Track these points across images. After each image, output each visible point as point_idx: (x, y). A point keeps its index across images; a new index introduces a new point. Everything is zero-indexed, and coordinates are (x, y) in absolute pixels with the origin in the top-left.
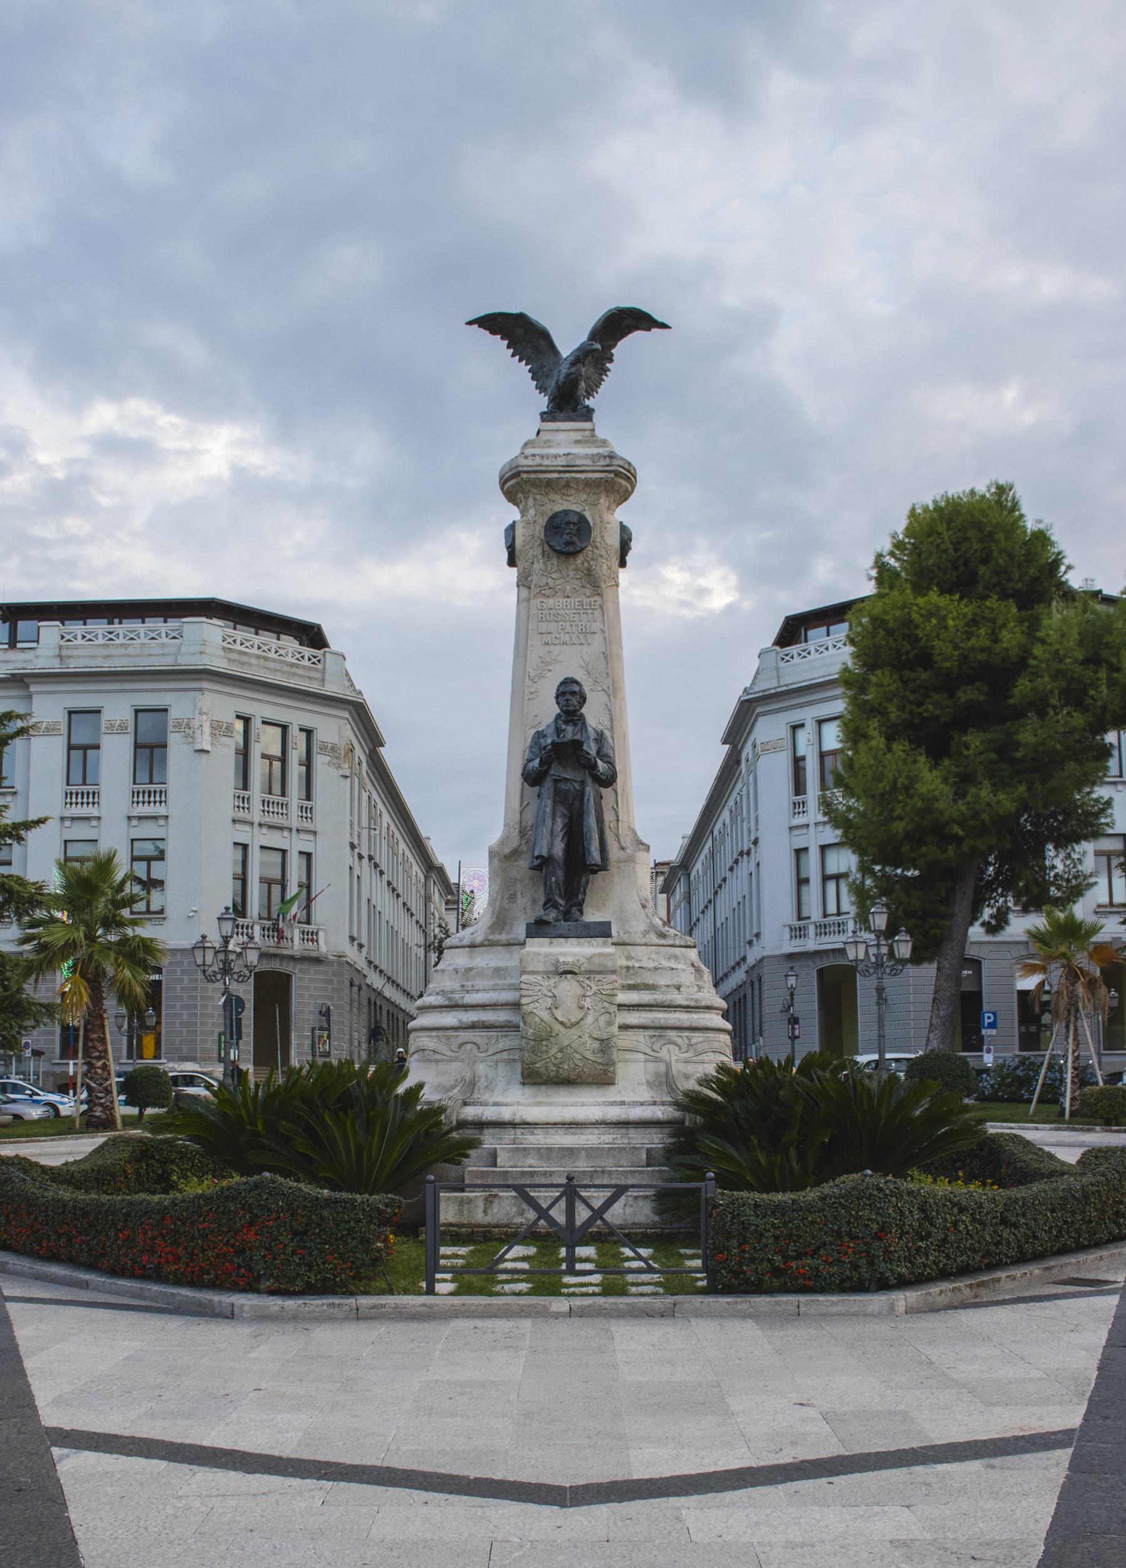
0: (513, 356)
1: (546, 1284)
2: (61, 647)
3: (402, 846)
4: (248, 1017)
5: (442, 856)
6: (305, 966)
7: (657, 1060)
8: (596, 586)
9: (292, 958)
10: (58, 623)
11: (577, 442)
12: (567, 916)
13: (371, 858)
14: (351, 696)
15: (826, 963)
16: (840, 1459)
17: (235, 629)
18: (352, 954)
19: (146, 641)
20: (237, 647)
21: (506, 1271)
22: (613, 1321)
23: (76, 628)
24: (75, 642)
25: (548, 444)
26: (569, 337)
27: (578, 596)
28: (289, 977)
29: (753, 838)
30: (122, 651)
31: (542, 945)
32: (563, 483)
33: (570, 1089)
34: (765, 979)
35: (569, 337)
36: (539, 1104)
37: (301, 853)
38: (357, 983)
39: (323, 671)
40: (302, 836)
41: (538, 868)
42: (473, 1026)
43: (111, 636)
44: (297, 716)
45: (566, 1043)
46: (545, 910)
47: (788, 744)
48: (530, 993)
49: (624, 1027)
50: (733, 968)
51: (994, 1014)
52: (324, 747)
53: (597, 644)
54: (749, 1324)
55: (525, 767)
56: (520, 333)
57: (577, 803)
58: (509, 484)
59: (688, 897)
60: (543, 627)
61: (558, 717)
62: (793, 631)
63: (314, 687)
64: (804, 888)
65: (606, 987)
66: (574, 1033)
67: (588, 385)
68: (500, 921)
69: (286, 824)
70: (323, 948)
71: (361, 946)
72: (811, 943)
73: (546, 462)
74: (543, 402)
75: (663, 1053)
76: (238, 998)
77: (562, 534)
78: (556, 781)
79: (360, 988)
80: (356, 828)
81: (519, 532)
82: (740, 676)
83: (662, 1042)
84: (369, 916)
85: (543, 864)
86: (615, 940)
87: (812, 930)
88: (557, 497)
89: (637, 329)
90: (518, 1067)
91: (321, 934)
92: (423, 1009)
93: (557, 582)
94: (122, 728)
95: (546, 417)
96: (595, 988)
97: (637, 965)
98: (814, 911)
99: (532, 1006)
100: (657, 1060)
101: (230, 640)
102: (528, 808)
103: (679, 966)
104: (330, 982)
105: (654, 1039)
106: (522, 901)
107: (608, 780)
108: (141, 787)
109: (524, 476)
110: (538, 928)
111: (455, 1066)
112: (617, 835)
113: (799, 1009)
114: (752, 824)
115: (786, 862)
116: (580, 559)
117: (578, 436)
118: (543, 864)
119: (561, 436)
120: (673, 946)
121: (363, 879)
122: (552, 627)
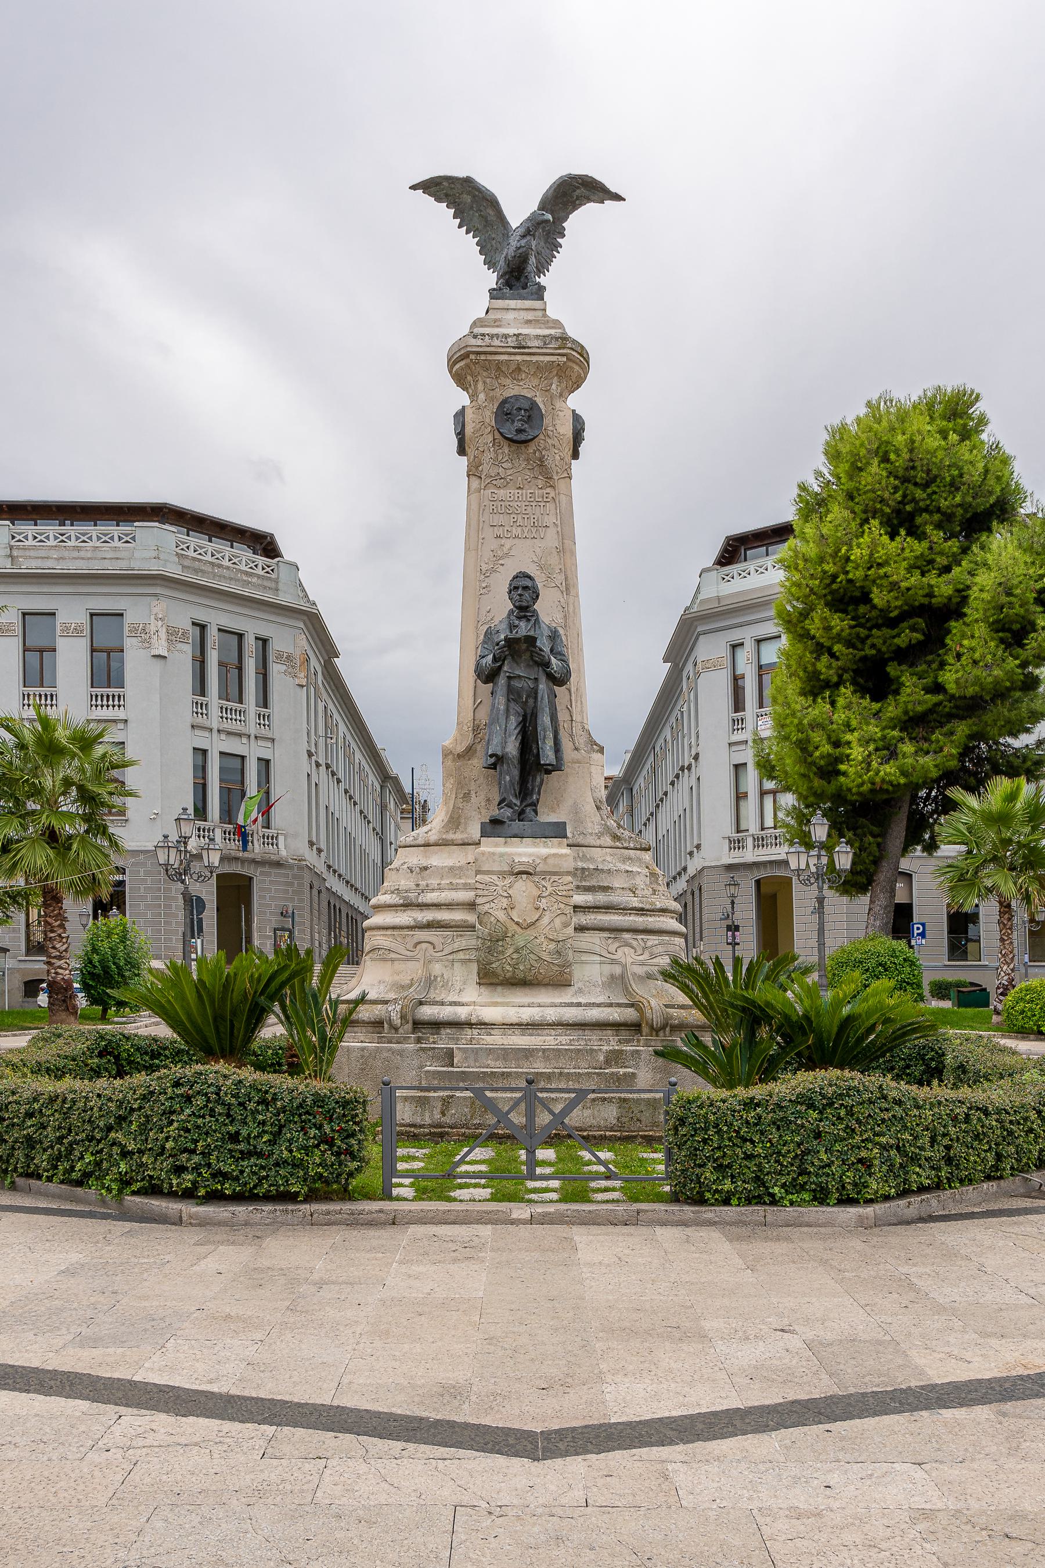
0: (460, 227)
1: (507, 1185)
2: (11, 548)
3: (358, 756)
4: (210, 917)
5: (397, 767)
6: (267, 869)
7: (613, 962)
8: (550, 477)
9: (254, 861)
10: (8, 522)
11: (528, 322)
12: (521, 815)
13: (328, 766)
14: (304, 606)
15: (763, 874)
16: (830, 1401)
17: (188, 535)
18: (311, 857)
19: (98, 544)
20: (191, 553)
21: (467, 1175)
22: (575, 1228)
23: (27, 528)
24: (27, 543)
25: (497, 323)
26: (518, 207)
27: (530, 488)
28: (251, 879)
29: (693, 753)
30: (76, 554)
31: (497, 845)
32: (513, 367)
33: (527, 990)
34: (704, 888)
35: (518, 207)
36: (495, 1004)
37: (259, 759)
38: (317, 886)
39: (276, 581)
40: (260, 743)
41: (493, 766)
42: (429, 925)
43: (63, 538)
44: (252, 626)
45: (522, 944)
46: (499, 809)
47: (728, 662)
48: (486, 893)
49: (581, 929)
50: (675, 878)
51: (923, 925)
52: (279, 656)
53: (551, 539)
55: (478, 665)
56: (464, 199)
57: (531, 701)
58: (457, 366)
59: (631, 812)
60: (498, 519)
61: (511, 612)
62: (735, 550)
63: (268, 596)
64: (742, 803)
65: (561, 888)
66: (531, 933)
67: (538, 261)
68: (455, 821)
69: (244, 730)
70: (284, 853)
71: (319, 851)
72: (750, 855)
73: (496, 342)
74: (491, 279)
76: (198, 898)
77: (513, 421)
78: (509, 678)
79: (319, 892)
80: (313, 737)
81: (469, 415)
83: (617, 944)
84: (327, 822)
85: (497, 762)
86: (570, 841)
87: (750, 841)
88: (507, 382)
89: (589, 200)
90: (474, 967)
91: (281, 839)
92: (379, 908)
93: (509, 472)
94: (78, 631)
95: (495, 294)
96: (550, 889)
97: (592, 867)
98: (751, 824)
99: (487, 906)
100: (613, 962)
101: (184, 546)
102: (481, 706)
103: (635, 869)
104: (291, 884)
105: (610, 941)
107: (560, 680)
109: (472, 357)
110: (494, 827)
111: (410, 964)
112: (571, 735)
114: (693, 740)
115: (726, 776)
116: (532, 447)
117: (530, 316)
118: (497, 762)
119: (511, 315)
120: (627, 848)
121: (320, 786)
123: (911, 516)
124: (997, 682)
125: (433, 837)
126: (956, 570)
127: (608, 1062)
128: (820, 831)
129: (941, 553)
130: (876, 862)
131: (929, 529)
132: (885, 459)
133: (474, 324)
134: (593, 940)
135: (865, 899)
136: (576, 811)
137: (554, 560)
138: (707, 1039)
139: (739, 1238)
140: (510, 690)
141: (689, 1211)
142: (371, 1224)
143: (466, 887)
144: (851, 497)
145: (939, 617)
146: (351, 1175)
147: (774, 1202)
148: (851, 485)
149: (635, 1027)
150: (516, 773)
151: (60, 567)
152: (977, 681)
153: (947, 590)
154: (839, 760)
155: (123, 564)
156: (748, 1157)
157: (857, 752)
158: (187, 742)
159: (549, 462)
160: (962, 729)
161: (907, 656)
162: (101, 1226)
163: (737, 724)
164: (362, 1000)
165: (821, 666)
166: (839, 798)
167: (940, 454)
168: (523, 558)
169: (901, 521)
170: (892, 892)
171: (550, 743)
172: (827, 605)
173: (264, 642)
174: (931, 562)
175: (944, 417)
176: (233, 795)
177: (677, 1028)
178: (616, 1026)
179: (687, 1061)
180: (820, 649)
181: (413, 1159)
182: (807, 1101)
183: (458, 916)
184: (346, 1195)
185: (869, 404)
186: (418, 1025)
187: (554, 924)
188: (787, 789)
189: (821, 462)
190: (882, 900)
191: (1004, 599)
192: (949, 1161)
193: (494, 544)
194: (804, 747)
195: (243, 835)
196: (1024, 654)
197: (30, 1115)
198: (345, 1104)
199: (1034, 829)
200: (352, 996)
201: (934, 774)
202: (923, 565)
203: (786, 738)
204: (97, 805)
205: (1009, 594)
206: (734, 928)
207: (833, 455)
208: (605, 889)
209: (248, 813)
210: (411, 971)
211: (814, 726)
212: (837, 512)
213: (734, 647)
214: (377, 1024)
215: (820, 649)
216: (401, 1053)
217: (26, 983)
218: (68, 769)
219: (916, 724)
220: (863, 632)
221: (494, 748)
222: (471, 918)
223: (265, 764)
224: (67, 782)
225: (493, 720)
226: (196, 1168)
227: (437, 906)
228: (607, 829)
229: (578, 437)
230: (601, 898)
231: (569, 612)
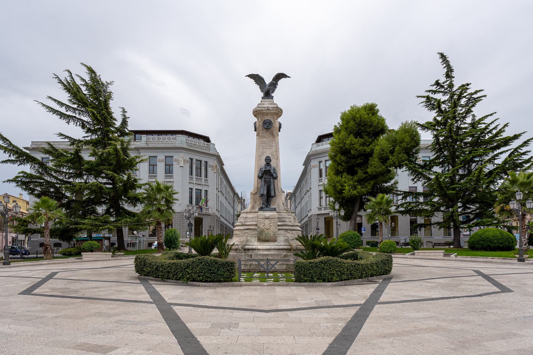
3: (228, 189)
5: (238, 191)
8: (274, 136)
12: (267, 207)
14: (216, 154)
18: (217, 213)
23: (150, 137)
25: (263, 104)
26: (268, 80)
35: (268, 80)
38: (218, 220)
42: (247, 229)
44: (203, 159)
49: (279, 230)
52: (210, 166)
53: (274, 149)
54: (303, 287)
56: (257, 79)
60: (263, 145)
62: (320, 139)
63: (207, 152)
66: (269, 230)
68: (253, 208)
72: (323, 212)
74: (262, 95)
75: (287, 235)
82: (307, 150)
85: (262, 195)
94: (162, 161)
95: (263, 98)
98: (324, 204)
106: (258, 203)
107: (276, 178)
108: (167, 175)
110: (261, 209)
113: (320, 226)
117: (270, 103)
119: (266, 103)
122: (264, 145)
123: (361, 133)
124: (380, 171)
125: (248, 211)
126: (371, 146)
127: (284, 257)
128: (337, 207)
129: (368, 142)
130: (352, 213)
131: (365, 136)
132: (354, 120)
133: (258, 105)
134: (282, 232)
135: (349, 222)
136: (278, 205)
137: (275, 153)
138: (305, 252)
139: (309, 289)
140: (265, 181)
141: (298, 283)
142: (236, 286)
143: (255, 221)
144: (346, 129)
145: (367, 156)
146: (232, 277)
147: (315, 282)
148: (347, 126)
149: (290, 250)
150: (266, 198)
151: (158, 146)
152: (376, 171)
153: (369, 150)
154: (343, 190)
155: (173, 145)
156: (310, 273)
157: (347, 188)
158: (188, 186)
159: (274, 133)
160: (372, 182)
161: (360, 165)
162: (185, 287)
163: (320, 180)
164: (233, 245)
165: (339, 168)
166: (343, 198)
167: (367, 119)
168: (268, 153)
169: (358, 134)
170: (356, 220)
171: (273, 191)
172: (341, 154)
173: (206, 162)
174: (365, 144)
175: (369, 110)
176: (198, 199)
177: (298, 250)
178: (286, 249)
179: (300, 256)
180: (339, 164)
181: (245, 275)
182: (321, 262)
183: (253, 227)
184: (231, 281)
185: (351, 107)
186: (245, 250)
187: (273, 229)
188: (331, 197)
189: (339, 121)
190: (353, 222)
191: (382, 152)
192: (351, 274)
193: (262, 150)
194: (335, 187)
195: (201, 208)
196: (387, 165)
197: (168, 267)
198: (232, 263)
199: (388, 206)
200: (231, 244)
201: (365, 193)
202: (363, 144)
203: (331, 185)
204: (169, 202)
205: (383, 151)
206: (318, 229)
207: (342, 119)
208: (284, 221)
209: (202, 203)
210: (243, 239)
211: (337, 182)
212: (343, 133)
213: (320, 162)
214: (236, 250)
215: (339, 164)
216: (241, 255)
217: (149, 244)
218: (163, 194)
219: (361, 181)
220: (349, 160)
221: (262, 193)
222: (256, 228)
223: (206, 191)
224: (163, 197)
225: (261, 187)
226: (203, 276)
227: (249, 225)
228: (285, 209)
229: (280, 127)
230: (283, 223)
231: (278, 164)
